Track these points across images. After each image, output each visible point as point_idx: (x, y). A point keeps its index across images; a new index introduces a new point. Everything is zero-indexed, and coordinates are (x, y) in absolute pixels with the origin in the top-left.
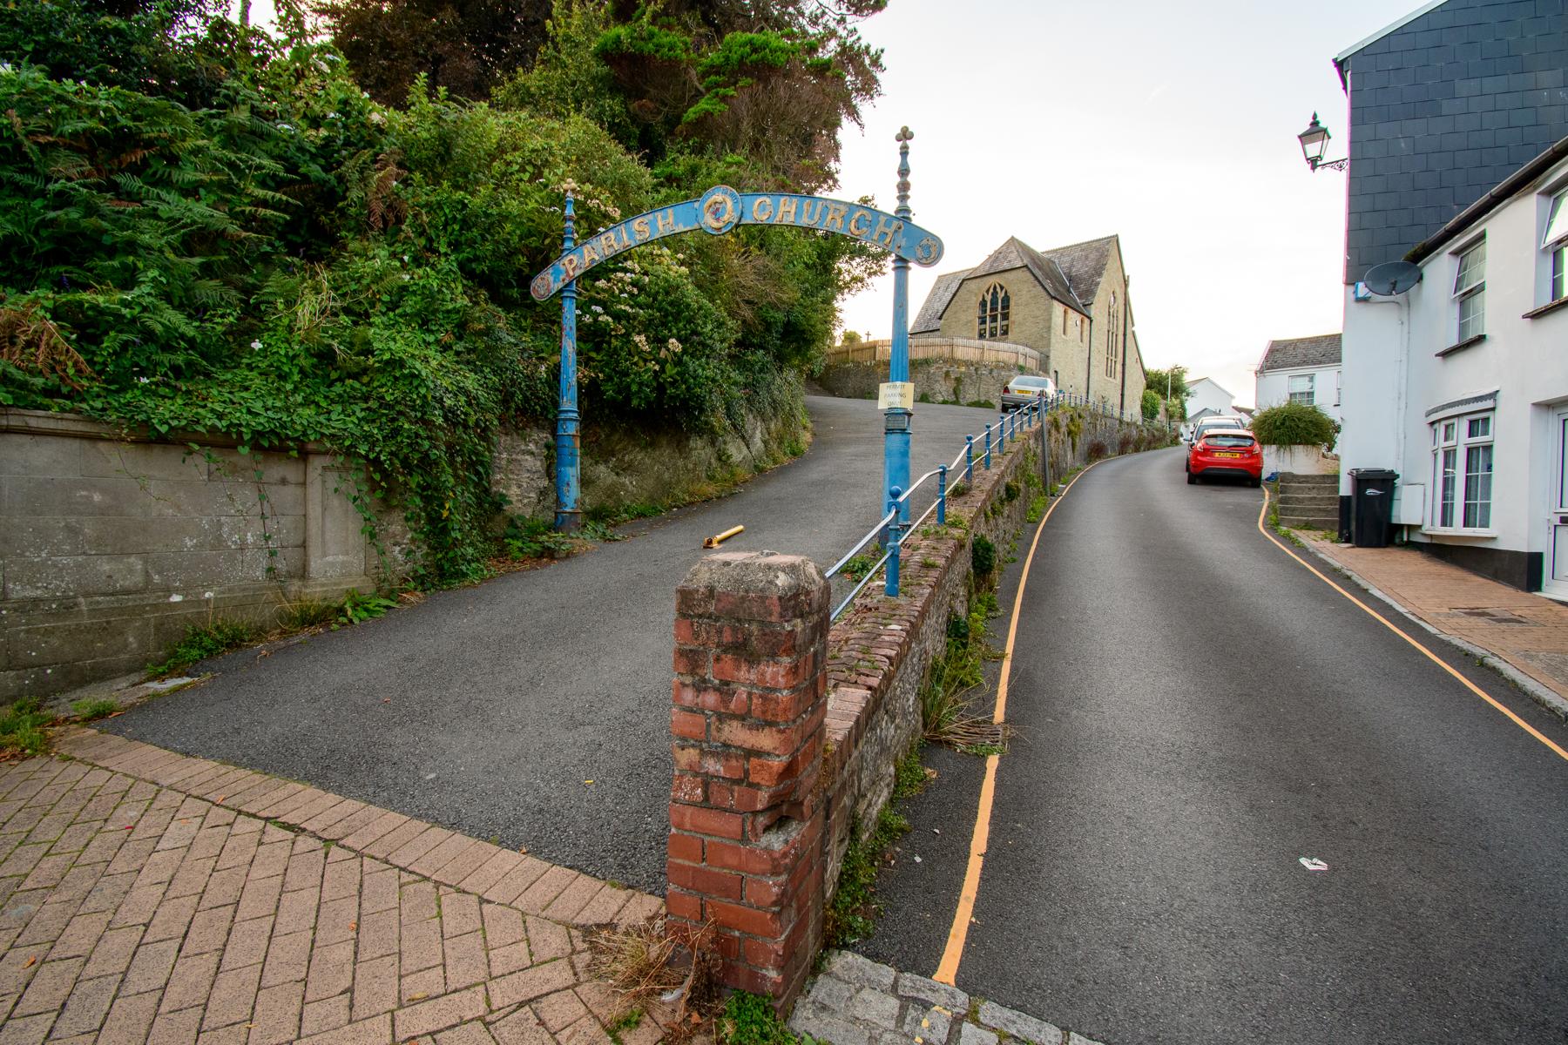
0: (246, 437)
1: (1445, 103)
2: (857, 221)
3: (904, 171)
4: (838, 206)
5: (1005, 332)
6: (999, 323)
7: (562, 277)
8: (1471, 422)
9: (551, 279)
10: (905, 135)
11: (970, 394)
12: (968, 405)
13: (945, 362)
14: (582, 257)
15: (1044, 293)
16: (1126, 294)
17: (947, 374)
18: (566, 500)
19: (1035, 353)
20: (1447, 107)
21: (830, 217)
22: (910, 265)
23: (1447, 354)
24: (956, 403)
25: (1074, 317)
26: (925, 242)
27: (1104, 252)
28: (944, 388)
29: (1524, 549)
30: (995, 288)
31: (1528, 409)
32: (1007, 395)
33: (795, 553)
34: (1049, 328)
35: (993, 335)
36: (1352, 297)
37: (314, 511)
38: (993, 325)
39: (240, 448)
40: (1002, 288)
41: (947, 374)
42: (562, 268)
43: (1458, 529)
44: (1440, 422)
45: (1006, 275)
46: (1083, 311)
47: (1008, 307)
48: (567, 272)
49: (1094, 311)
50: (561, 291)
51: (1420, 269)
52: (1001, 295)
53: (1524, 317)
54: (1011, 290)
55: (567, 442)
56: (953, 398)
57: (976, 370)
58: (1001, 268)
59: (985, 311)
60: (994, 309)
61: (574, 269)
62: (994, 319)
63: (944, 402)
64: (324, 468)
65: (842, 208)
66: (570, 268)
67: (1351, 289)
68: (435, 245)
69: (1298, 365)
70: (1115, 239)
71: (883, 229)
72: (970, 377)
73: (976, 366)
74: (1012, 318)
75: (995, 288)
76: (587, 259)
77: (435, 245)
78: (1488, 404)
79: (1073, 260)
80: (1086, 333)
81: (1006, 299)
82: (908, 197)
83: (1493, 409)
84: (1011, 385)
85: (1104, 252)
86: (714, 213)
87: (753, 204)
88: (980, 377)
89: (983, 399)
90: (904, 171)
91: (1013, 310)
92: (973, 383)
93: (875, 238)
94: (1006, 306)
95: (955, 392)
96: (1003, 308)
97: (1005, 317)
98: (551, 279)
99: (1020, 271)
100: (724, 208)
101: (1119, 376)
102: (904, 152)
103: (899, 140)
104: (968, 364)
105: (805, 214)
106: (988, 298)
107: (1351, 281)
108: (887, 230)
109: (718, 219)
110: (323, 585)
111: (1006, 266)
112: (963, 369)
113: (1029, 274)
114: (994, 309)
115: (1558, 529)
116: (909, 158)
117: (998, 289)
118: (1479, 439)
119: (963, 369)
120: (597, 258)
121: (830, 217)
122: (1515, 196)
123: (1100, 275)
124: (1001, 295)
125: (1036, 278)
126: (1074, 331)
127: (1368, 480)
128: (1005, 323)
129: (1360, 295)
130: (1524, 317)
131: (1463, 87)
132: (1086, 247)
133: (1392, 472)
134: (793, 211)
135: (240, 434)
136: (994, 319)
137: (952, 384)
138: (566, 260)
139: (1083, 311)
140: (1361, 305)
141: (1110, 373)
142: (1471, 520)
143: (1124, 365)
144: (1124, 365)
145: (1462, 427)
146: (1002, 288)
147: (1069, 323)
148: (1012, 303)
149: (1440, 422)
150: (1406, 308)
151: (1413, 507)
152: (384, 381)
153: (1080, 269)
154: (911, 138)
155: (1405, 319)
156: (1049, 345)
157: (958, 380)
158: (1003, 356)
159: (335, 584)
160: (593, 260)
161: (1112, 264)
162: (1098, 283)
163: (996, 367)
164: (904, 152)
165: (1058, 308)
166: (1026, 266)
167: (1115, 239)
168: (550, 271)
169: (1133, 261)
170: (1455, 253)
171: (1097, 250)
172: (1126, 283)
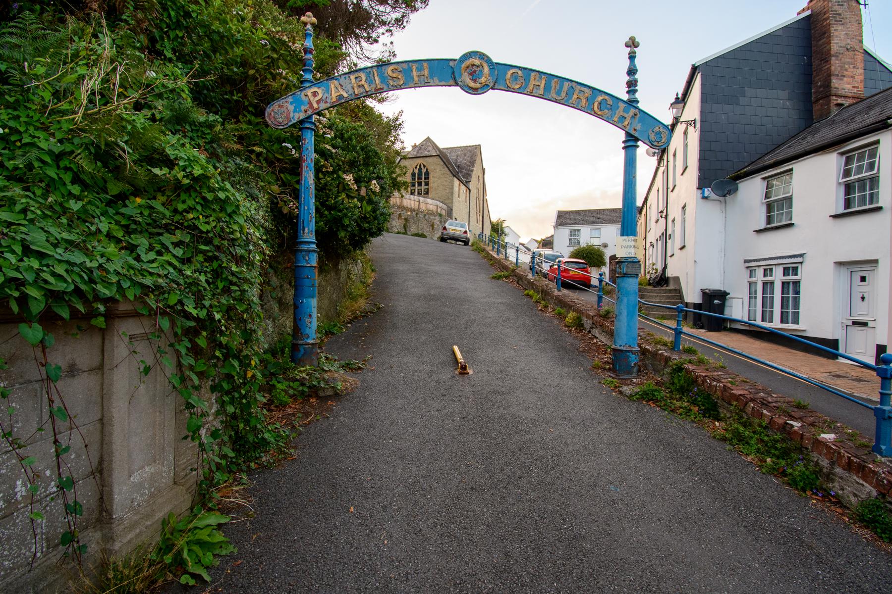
0: (36, 308)
1: (741, 98)
2: (600, 104)
3: (632, 72)
4: (583, 89)
5: (427, 193)
6: (423, 187)
7: (303, 108)
8: (784, 269)
9: (291, 108)
10: (632, 44)
11: (413, 229)
12: (412, 235)
13: (399, 207)
14: (328, 90)
15: (449, 173)
16: (483, 178)
17: (400, 215)
18: (307, 331)
19: (445, 207)
20: (742, 100)
21: (575, 96)
22: (640, 143)
23: (759, 231)
24: (405, 233)
25: (463, 188)
26: (657, 129)
27: (473, 153)
28: (398, 224)
29: (831, 338)
30: (420, 166)
31: (832, 264)
32: (445, 231)
33: (464, 357)
34: (452, 193)
35: (419, 194)
36: (700, 196)
37: (119, 409)
38: (419, 188)
39: (23, 328)
40: (424, 166)
41: (400, 215)
42: (303, 98)
43: (776, 324)
44: (750, 266)
45: (427, 159)
46: (466, 184)
47: (428, 178)
48: (310, 103)
49: (471, 186)
50: (302, 122)
51: (737, 184)
52: (424, 171)
53: (830, 216)
54: (430, 168)
55: (306, 273)
56: (403, 230)
57: (417, 214)
58: (424, 155)
59: (415, 179)
60: (420, 178)
61: (318, 102)
62: (420, 184)
63: (399, 233)
64: (131, 337)
65: (586, 90)
66: (314, 101)
67: (700, 191)
68: (158, 46)
69: (573, 224)
70: (478, 147)
71: (622, 113)
72: (413, 218)
73: (416, 211)
74: (431, 185)
75: (420, 166)
76: (334, 95)
77: (158, 46)
78: (799, 260)
79: (457, 155)
80: (468, 198)
81: (427, 173)
82: (636, 91)
83: (801, 263)
84: (447, 225)
85: (473, 153)
86: (472, 74)
87: (506, 74)
88: (418, 219)
89: (420, 232)
90: (632, 72)
91: (431, 180)
92: (414, 222)
93: (616, 119)
94: (427, 177)
95: (405, 227)
96: (425, 179)
97: (427, 184)
98: (291, 108)
99: (435, 158)
100: (482, 72)
101: (481, 223)
102: (632, 57)
103: (627, 46)
104: (412, 210)
105: (553, 91)
106: (417, 171)
107: (700, 187)
108: (626, 115)
109: (475, 81)
110: (132, 527)
111: (426, 153)
112: (409, 213)
113: (440, 160)
114: (420, 178)
115: (848, 328)
116: (636, 61)
117: (422, 167)
118: (768, 279)
119: (409, 213)
120: (345, 95)
121: (575, 96)
122: (820, 152)
123: (473, 166)
124: (424, 171)
125: (445, 163)
126: (463, 196)
127: (715, 296)
128: (426, 187)
129: (706, 195)
130: (830, 216)
131: (749, 92)
132: (465, 149)
133: (725, 292)
134: (542, 86)
135: (23, 300)
136: (420, 184)
137: (403, 222)
138: (309, 92)
139: (466, 184)
140: (704, 200)
141: (477, 221)
142: (785, 319)
143: (483, 217)
144: (483, 217)
145: (760, 272)
146: (424, 166)
147: (461, 191)
148: (431, 176)
149: (750, 266)
150: (724, 204)
151: (737, 310)
152: (190, 203)
153: (462, 161)
154: (636, 47)
155: (724, 210)
156: (452, 202)
157: (406, 220)
158: (430, 207)
159: (147, 516)
160: (341, 96)
161: (478, 161)
162: (472, 171)
163: (428, 213)
164: (632, 57)
165: (456, 182)
166: (438, 155)
167: (478, 147)
168: (290, 99)
169: (488, 158)
170: (764, 179)
171: (470, 152)
172: (484, 173)
